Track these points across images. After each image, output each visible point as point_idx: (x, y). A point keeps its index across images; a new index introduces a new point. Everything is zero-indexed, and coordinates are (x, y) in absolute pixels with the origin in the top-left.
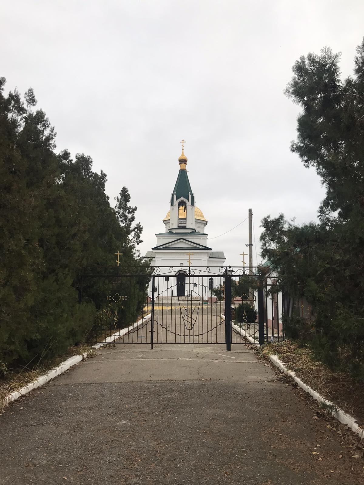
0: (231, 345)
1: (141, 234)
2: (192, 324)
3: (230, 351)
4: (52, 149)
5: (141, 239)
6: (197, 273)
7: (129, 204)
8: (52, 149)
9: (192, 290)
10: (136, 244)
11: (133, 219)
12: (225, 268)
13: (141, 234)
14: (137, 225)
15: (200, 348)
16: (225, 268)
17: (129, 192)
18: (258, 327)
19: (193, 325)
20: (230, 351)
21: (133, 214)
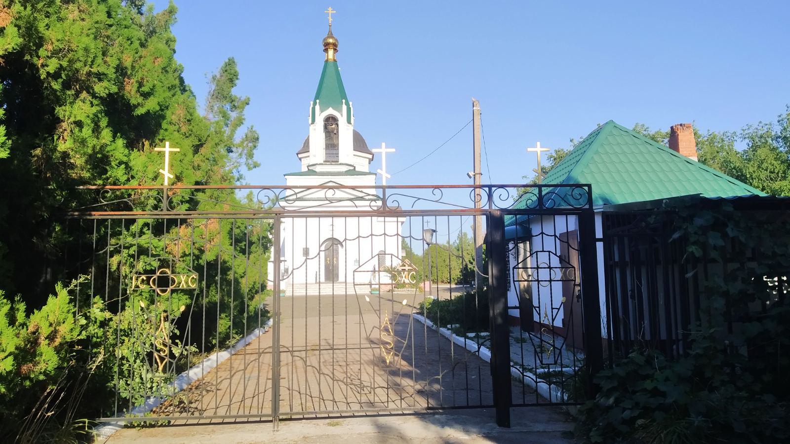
0: (511, 409)
1: (254, 151)
2: (554, 347)
3: (508, 426)
4: (144, 357)
5: (255, 159)
6: (406, 205)
7: (235, 92)
8: (144, 357)
9: (392, 255)
10: (243, 169)
11: (240, 122)
12: (487, 189)
13: (254, 151)
14: (183, 253)
15: (437, 416)
16: (487, 189)
17: (238, 69)
18: (512, 355)
19: (557, 352)
20: (508, 426)
21: (241, 112)
